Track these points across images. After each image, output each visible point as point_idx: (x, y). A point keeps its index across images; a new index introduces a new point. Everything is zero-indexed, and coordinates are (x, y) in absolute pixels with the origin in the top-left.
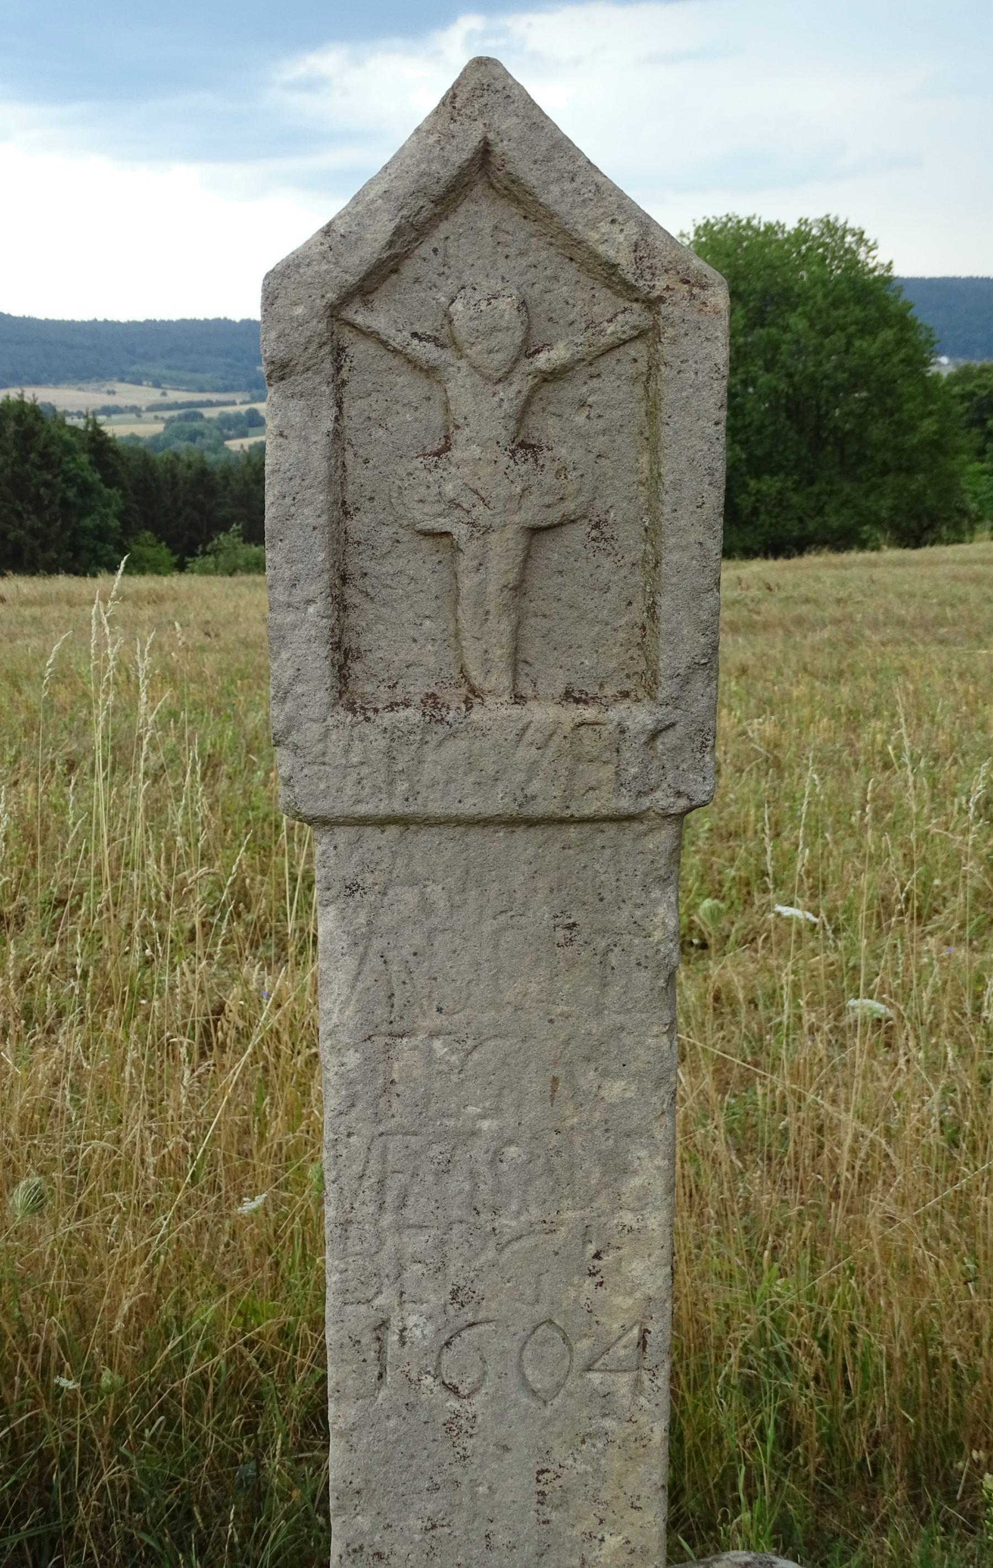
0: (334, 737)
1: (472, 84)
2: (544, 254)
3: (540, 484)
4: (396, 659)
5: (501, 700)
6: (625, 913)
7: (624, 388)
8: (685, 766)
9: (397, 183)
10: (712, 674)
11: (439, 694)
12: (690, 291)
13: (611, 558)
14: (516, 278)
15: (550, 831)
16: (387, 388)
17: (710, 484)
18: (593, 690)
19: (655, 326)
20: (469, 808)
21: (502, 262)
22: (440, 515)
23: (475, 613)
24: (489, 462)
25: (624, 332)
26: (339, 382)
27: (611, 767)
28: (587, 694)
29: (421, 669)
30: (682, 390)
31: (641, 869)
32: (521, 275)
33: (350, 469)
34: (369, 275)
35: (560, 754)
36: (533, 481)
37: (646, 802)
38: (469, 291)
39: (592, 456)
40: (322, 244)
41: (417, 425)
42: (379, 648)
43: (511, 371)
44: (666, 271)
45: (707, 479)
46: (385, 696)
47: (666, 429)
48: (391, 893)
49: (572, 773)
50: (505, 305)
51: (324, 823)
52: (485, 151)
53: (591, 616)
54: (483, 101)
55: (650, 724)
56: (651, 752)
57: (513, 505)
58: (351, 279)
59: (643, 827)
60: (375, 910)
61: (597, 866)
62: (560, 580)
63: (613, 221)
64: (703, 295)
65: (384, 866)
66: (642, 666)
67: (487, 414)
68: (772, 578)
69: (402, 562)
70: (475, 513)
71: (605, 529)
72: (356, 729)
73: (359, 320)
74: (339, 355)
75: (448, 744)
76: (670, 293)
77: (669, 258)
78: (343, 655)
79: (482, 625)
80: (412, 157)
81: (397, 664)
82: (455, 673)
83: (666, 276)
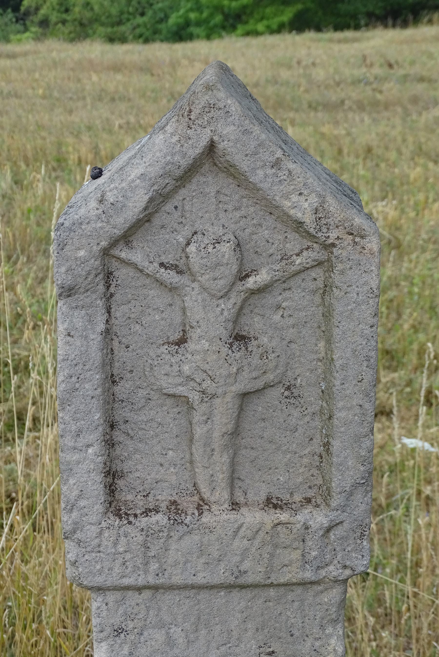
0: (106, 535)
1: (203, 104)
2: (252, 209)
3: (249, 364)
4: (148, 477)
5: (222, 508)
6: (308, 644)
7: (308, 297)
8: (349, 549)
9: (150, 169)
10: (368, 489)
11: (179, 502)
12: (353, 240)
13: (298, 409)
14: (232, 226)
15: (256, 591)
16: (142, 298)
17: (367, 367)
18: (286, 497)
19: (329, 260)
20: (200, 579)
21: (222, 215)
22: (180, 385)
23: (205, 451)
24: (214, 352)
25: (308, 263)
26: (109, 295)
27: (299, 552)
28: (282, 501)
29: (166, 484)
30: (348, 305)
31: (319, 615)
32: (236, 223)
33: (116, 352)
34: (130, 228)
35: (264, 544)
36: (245, 362)
37: (323, 573)
38: (200, 236)
39: (285, 342)
40: (97, 209)
41: (163, 322)
42: (137, 470)
43: (229, 290)
44: (337, 227)
45: (365, 364)
46: (141, 503)
47: (337, 330)
48: (146, 633)
49: (272, 555)
50: (226, 249)
51: (99, 589)
52: (211, 147)
53: (284, 448)
54: (210, 115)
55: (326, 523)
56: (326, 540)
57: (232, 380)
58: (118, 232)
59: (320, 588)
60: (134, 645)
61: (289, 613)
62: (263, 424)
63: (300, 194)
64: (363, 242)
65: (141, 616)
66: (320, 481)
67: (212, 320)
68: (392, 54)
69: (152, 413)
70: (204, 385)
71: (294, 391)
72: (122, 529)
73: (123, 255)
74: (108, 277)
75: (186, 538)
76: (340, 241)
77: (339, 219)
78: (112, 477)
79: (209, 458)
80: (161, 151)
81: (149, 480)
82: (192, 489)
83: (336, 230)
